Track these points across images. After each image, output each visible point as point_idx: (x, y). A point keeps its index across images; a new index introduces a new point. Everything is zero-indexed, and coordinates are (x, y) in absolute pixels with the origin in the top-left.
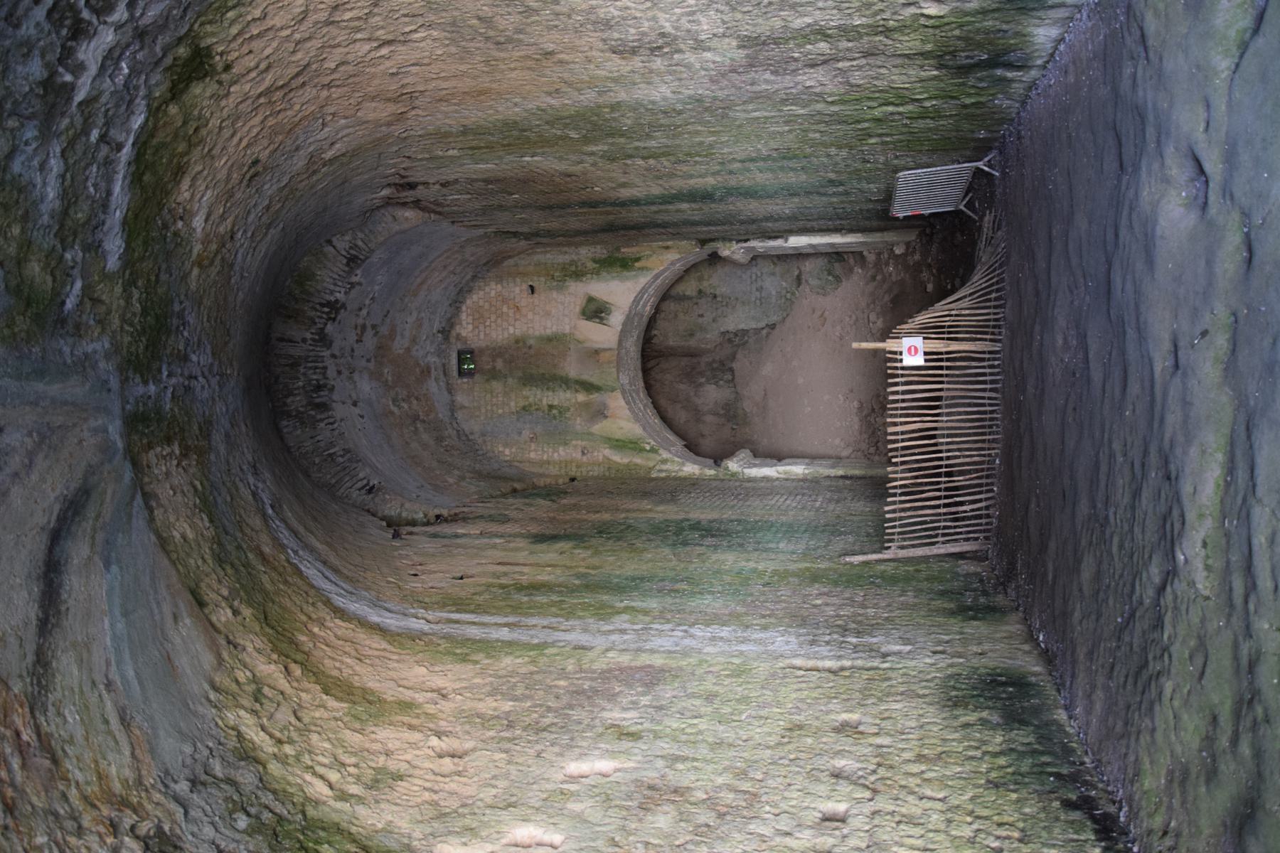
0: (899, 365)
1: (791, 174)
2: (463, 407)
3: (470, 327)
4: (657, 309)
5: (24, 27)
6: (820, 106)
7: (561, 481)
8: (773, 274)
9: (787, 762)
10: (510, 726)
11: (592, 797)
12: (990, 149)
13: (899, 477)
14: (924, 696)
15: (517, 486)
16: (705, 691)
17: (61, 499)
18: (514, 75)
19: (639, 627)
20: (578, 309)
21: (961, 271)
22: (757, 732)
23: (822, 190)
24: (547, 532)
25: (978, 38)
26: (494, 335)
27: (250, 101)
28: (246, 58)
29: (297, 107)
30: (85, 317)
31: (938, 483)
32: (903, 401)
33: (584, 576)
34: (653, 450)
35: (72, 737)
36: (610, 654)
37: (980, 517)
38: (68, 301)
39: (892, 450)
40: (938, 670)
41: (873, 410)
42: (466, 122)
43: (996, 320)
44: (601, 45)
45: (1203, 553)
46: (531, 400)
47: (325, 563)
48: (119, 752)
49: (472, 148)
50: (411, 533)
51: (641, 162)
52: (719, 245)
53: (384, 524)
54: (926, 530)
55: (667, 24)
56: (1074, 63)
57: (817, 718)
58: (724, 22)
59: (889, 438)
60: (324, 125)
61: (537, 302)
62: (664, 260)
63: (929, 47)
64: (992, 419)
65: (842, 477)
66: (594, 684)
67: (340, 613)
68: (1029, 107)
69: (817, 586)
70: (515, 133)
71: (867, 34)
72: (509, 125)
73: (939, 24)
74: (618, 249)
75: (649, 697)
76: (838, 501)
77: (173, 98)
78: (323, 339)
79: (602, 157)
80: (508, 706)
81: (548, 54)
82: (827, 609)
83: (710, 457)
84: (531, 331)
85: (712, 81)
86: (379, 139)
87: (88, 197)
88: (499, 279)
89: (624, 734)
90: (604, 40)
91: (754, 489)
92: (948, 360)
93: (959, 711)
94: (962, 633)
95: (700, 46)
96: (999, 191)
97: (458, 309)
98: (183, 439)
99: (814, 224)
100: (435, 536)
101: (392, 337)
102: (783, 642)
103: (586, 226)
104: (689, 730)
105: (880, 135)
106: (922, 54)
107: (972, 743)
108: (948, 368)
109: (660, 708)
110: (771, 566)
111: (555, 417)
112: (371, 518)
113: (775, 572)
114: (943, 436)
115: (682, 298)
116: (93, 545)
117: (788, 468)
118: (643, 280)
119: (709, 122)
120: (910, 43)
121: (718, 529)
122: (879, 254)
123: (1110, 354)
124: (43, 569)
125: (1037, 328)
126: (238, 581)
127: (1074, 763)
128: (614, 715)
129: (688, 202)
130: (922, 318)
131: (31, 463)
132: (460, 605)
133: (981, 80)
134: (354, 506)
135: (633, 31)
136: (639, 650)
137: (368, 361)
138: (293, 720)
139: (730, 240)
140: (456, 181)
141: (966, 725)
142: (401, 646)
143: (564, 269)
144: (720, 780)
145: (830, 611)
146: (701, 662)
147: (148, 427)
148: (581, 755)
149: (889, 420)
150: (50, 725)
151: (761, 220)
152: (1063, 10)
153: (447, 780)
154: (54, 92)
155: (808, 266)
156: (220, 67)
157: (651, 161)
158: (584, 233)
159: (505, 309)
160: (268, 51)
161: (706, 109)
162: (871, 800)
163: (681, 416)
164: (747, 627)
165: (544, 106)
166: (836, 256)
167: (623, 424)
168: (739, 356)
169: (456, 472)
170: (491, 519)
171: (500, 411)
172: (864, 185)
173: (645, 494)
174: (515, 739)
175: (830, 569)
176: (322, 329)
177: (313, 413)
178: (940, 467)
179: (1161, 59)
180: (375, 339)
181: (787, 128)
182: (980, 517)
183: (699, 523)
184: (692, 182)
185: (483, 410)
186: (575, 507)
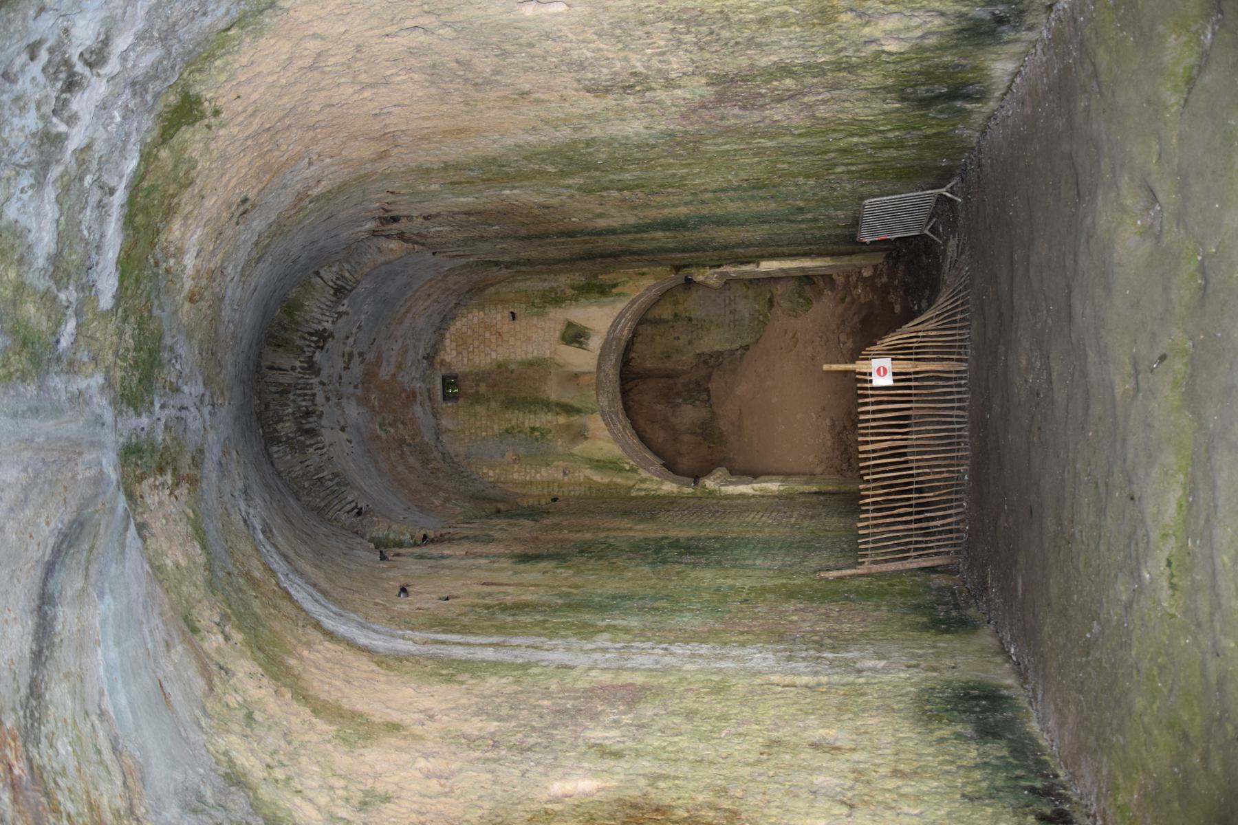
0: (868, 385)
1: (762, 203)
2: (448, 431)
3: (454, 353)
4: (635, 334)
5: (20, 82)
6: (787, 139)
7: (543, 502)
8: (746, 297)
9: (766, 779)
10: (496, 745)
11: (576, 817)
12: (952, 176)
13: (872, 496)
14: (900, 711)
15: (501, 506)
16: (686, 708)
17: (56, 532)
18: (492, 113)
19: (622, 645)
20: (558, 334)
21: (927, 292)
22: (737, 748)
23: (792, 218)
24: (531, 552)
25: (937, 72)
26: (477, 360)
27: (237, 144)
28: (234, 103)
29: (284, 148)
30: (79, 355)
31: (909, 499)
32: (874, 420)
33: (568, 595)
34: (633, 470)
35: (64, 769)
36: (593, 673)
37: (951, 531)
38: (62, 340)
39: (863, 468)
40: (913, 685)
41: (845, 428)
42: (444, 158)
43: (961, 341)
44: (575, 85)
45: (1168, 571)
46: (513, 423)
47: (314, 586)
48: (111, 782)
49: (453, 183)
50: (398, 555)
51: (615, 194)
52: (693, 270)
53: (372, 546)
54: (898, 545)
55: (638, 64)
56: (1030, 95)
57: (795, 735)
58: (693, 62)
59: (861, 456)
60: (310, 164)
61: (518, 328)
62: (639, 287)
63: (890, 82)
64: (959, 437)
65: (816, 493)
66: (576, 703)
67: (331, 635)
68: (988, 137)
69: (793, 601)
70: (494, 168)
71: (832, 71)
72: (487, 161)
73: (901, 58)
74: (596, 276)
75: (631, 716)
76: (812, 517)
77: (163, 143)
78: (312, 367)
79: (578, 189)
80: (493, 726)
81: (524, 94)
82: (804, 625)
83: (688, 476)
84: (512, 356)
85: (683, 116)
86: (364, 176)
87: (82, 239)
88: (481, 307)
89: (605, 753)
90: (578, 81)
91: (731, 506)
92: (916, 380)
93: (935, 725)
94: (934, 647)
95: (670, 84)
96: (962, 216)
97: (443, 335)
98: (174, 469)
99: (785, 249)
100: (421, 557)
101: (378, 362)
102: (761, 658)
103: (565, 255)
104: (670, 749)
105: (847, 165)
106: (884, 88)
107: (948, 758)
108: (916, 387)
109: (642, 726)
110: (748, 583)
111: (537, 439)
112: (359, 540)
113: (752, 589)
114: (913, 454)
115: (657, 322)
116: (87, 576)
117: (763, 485)
118: (621, 305)
119: (681, 155)
120: (872, 78)
121: (697, 547)
122: (848, 277)
123: (1072, 376)
124: (37, 602)
125: (1002, 349)
126: (230, 606)
127: (1048, 776)
128: (597, 734)
129: (664, 230)
130: (890, 340)
131: (26, 497)
132: (446, 625)
133: (941, 112)
134: (343, 527)
135: (605, 71)
136: (620, 669)
137: (356, 387)
138: (283, 743)
139: (704, 266)
140: (439, 214)
141: (942, 740)
142: (389, 667)
143: (543, 296)
144: (701, 798)
145: (806, 627)
146: (681, 680)
147: (141, 458)
148: (565, 774)
149: (860, 439)
150: (42, 755)
151: (733, 247)
152: (1019, 44)
153: (434, 801)
154: (50, 141)
155: (779, 289)
156: (209, 112)
157: (626, 193)
158: (564, 261)
159: (487, 336)
160: (255, 96)
161: (678, 144)
162: (849, 816)
163: (659, 436)
164: (726, 644)
165: (521, 142)
166: (806, 279)
167: (602, 444)
168: (714, 376)
169: (442, 494)
170: (476, 539)
171: (484, 434)
172: (832, 212)
173: (625, 513)
174: (500, 759)
175: (806, 585)
176: (311, 358)
177: (302, 438)
178: (911, 483)
179: (1113, 95)
180: (362, 366)
181: (756, 160)
182: (951, 531)
183: (678, 540)
184: (666, 211)
185: (467, 433)
186: (558, 527)
